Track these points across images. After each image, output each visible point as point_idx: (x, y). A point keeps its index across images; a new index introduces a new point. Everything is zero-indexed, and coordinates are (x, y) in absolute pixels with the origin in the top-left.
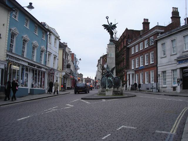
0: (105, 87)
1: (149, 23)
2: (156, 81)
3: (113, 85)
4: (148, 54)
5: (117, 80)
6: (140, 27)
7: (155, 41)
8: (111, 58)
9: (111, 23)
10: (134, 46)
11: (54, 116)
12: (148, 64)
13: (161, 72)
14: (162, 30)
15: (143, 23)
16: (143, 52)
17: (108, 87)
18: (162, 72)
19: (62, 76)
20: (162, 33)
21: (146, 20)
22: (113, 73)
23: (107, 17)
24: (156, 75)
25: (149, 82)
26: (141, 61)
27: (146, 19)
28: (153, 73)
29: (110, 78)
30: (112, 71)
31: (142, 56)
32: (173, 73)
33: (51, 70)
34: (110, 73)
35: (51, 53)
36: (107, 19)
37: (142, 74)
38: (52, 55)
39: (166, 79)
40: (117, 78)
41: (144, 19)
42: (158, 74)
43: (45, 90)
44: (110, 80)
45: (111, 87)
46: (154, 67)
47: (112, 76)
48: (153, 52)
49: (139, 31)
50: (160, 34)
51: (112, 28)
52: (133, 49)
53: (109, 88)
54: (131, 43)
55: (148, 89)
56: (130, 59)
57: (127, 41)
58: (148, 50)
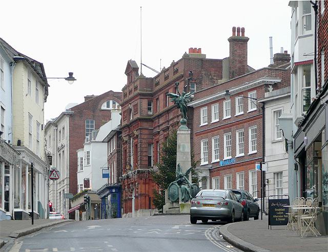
0: (177, 201)
1: (247, 40)
4: (243, 130)
6: (218, 50)
8: (184, 153)
10: (208, 104)
12: (243, 154)
13: (273, 173)
14: (276, 77)
15: (231, 40)
16: (232, 125)
17: (183, 200)
18: (274, 173)
20: (275, 86)
21: (238, 32)
26: (225, 146)
27: (239, 29)
29: (186, 187)
30: (187, 175)
31: (230, 134)
32: (278, 179)
33: (52, 172)
37: (229, 179)
39: (282, 189)
41: (234, 29)
42: (266, 178)
44: (186, 189)
45: (187, 201)
46: (255, 118)
47: (188, 183)
49: (221, 61)
50: (271, 88)
52: (203, 112)
53: (183, 203)
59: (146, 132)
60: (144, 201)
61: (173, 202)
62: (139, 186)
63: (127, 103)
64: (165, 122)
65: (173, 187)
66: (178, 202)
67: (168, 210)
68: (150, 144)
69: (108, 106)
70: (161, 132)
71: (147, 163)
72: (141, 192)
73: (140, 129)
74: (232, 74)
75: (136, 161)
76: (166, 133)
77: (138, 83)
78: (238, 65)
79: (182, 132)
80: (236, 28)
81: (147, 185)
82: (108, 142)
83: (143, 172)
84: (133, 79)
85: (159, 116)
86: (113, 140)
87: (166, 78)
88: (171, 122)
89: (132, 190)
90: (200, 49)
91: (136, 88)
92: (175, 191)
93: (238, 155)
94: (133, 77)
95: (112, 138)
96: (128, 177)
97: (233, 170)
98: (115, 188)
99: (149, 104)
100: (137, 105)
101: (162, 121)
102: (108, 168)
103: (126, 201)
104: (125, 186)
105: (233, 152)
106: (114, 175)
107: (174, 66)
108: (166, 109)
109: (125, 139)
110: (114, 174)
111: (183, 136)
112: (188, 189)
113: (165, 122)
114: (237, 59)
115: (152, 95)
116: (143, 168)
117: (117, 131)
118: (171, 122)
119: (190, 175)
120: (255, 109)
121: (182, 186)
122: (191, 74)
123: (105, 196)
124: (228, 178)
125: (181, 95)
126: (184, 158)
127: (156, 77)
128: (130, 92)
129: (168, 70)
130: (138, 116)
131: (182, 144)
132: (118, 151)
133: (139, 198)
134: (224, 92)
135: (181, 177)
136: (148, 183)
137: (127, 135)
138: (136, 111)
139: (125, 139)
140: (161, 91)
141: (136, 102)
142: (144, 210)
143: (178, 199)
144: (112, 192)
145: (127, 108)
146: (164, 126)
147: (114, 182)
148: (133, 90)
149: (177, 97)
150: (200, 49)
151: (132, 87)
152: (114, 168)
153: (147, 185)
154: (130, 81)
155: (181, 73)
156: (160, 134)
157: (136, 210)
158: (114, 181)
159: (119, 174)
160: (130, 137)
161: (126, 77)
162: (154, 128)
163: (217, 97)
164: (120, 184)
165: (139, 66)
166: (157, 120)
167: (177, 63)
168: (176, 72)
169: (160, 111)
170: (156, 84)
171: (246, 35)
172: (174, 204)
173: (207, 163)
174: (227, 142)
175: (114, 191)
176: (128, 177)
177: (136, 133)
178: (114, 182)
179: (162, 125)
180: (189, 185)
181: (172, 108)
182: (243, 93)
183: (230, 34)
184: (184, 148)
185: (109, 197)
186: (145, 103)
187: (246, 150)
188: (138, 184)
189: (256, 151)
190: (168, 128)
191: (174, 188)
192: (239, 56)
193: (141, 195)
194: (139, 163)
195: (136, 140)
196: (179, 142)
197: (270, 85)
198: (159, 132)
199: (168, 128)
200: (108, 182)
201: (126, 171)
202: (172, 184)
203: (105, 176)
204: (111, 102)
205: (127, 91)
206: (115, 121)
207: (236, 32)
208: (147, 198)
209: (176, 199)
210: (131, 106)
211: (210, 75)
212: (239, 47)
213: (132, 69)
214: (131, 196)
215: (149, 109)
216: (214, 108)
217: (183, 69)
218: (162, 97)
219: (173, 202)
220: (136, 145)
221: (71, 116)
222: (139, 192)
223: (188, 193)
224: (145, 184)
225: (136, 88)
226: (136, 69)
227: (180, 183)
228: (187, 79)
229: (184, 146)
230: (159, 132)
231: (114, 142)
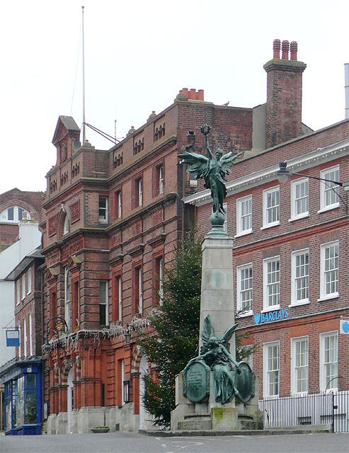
0: (205, 401)
1: (301, 68)
3: (234, 391)
4: (306, 251)
5: (246, 376)
12: (306, 301)
15: (271, 68)
17: (218, 399)
21: (285, 51)
22: (228, 346)
25: (314, 387)
27: (285, 43)
28: (335, 348)
29: (226, 369)
34: (220, 351)
37: (274, 351)
41: (277, 43)
45: (228, 401)
48: (335, 244)
52: (242, 208)
53: (219, 405)
55: (305, 421)
59: (95, 258)
61: (193, 404)
62: (83, 363)
63: (57, 202)
64: (136, 238)
65: (196, 368)
66: (207, 403)
67: (183, 420)
68: (103, 281)
69: (11, 217)
70: (127, 258)
71: (97, 318)
72: (86, 373)
73: (85, 251)
74: (272, 139)
75: (75, 315)
76: (136, 260)
77: (80, 160)
78: (285, 120)
79: (214, 244)
80: (282, 42)
81: (98, 362)
82: (15, 280)
83: (90, 336)
84: (69, 153)
85: (124, 225)
86: (27, 276)
87: (138, 148)
88: (149, 238)
89: (67, 370)
90: (201, 92)
91: (75, 171)
92: (199, 377)
93: (295, 302)
94: (69, 149)
95: (25, 271)
96: (59, 345)
97: (282, 333)
98: (33, 364)
99: (102, 204)
100: (77, 204)
101: (127, 235)
102: (17, 328)
103: (55, 390)
104: (53, 362)
105: (283, 294)
106: (28, 341)
107: (155, 122)
108: (137, 210)
109: (54, 272)
110: (29, 339)
111: (217, 253)
112: (230, 374)
113: (136, 238)
114: (283, 107)
115: (107, 185)
116: (91, 327)
117: (35, 258)
118: (149, 238)
119: (232, 342)
120: (337, 205)
121: (218, 367)
123: (12, 380)
124: (270, 348)
125: (214, 156)
126: (220, 303)
127: (114, 150)
128: (63, 180)
129: (141, 131)
130: (80, 226)
131: (214, 271)
132: (39, 297)
133: (83, 386)
134: (275, 168)
135: (213, 345)
136: (101, 358)
137: (57, 265)
138: (76, 217)
139: (54, 272)
140: (125, 176)
141: (76, 199)
142: (93, 409)
143: (208, 395)
144: (26, 374)
145: (58, 211)
146: (132, 246)
147: (29, 354)
148: (69, 176)
149: (203, 161)
150: (201, 92)
151: (67, 169)
152: (28, 328)
153: (98, 362)
154: (63, 158)
155: (171, 133)
156: (125, 261)
157: (76, 406)
158: (29, 352)
159: (39, 341)
160: (63, 269)
161: (54, 150)
162: (112, 250)
163: (249, 183)
164: (40, 357)
165: (80, 126)
166: (118, 235)
167: (162, 115)
168: (160, 133)
169: (145, 205)
170: (115, 163)
171: (301, 57)
172: (198, 407)
174: (242, 282)
175: (29, 370)
176: (59, 345)
177: (76, 259)
178: (29, 354)
179: (149, 232)
180: (231, 366)
181: (150, 209)
182: (311, 172)
183: (269, 56)
184: (218, 281)
185: (21, 380)
186: (93, 199)
187: (314, 292)
188: (81, 358)
189: (336, 295)
190: (142, 249)
191: (198, 371)
192: (287, 101)
193: (86, 380)
194: (82, 319)
195: (77, 274)
196: (206, 266)
198: (122, 258)
199: (142, 249)
200: (17, 354)
201: (54, 332)
202: (194, 363)
203: (11, 342)
204: (16, 210)
205: (57, 178)
206: (31, 239)
207: (281, 51)
208: (98, 385)
209: (203, 395)
210: (65, 207)
211: (229, 140)
212: (287, 82)
213: (66, 134)
214: (66, 381)
215: (102, 213)
216: (297, 189)
217: (176, 124)
218: (127, 187)
219: (193, 404)
220: (77, 284)
222: (83, 374)
223: (230, 382)
224: (94, 358)
225: (75, 171)
226: (75, 133)
227: (211, 360)
229: (219, 274)
230: (122, 258)
231: (29, 281)
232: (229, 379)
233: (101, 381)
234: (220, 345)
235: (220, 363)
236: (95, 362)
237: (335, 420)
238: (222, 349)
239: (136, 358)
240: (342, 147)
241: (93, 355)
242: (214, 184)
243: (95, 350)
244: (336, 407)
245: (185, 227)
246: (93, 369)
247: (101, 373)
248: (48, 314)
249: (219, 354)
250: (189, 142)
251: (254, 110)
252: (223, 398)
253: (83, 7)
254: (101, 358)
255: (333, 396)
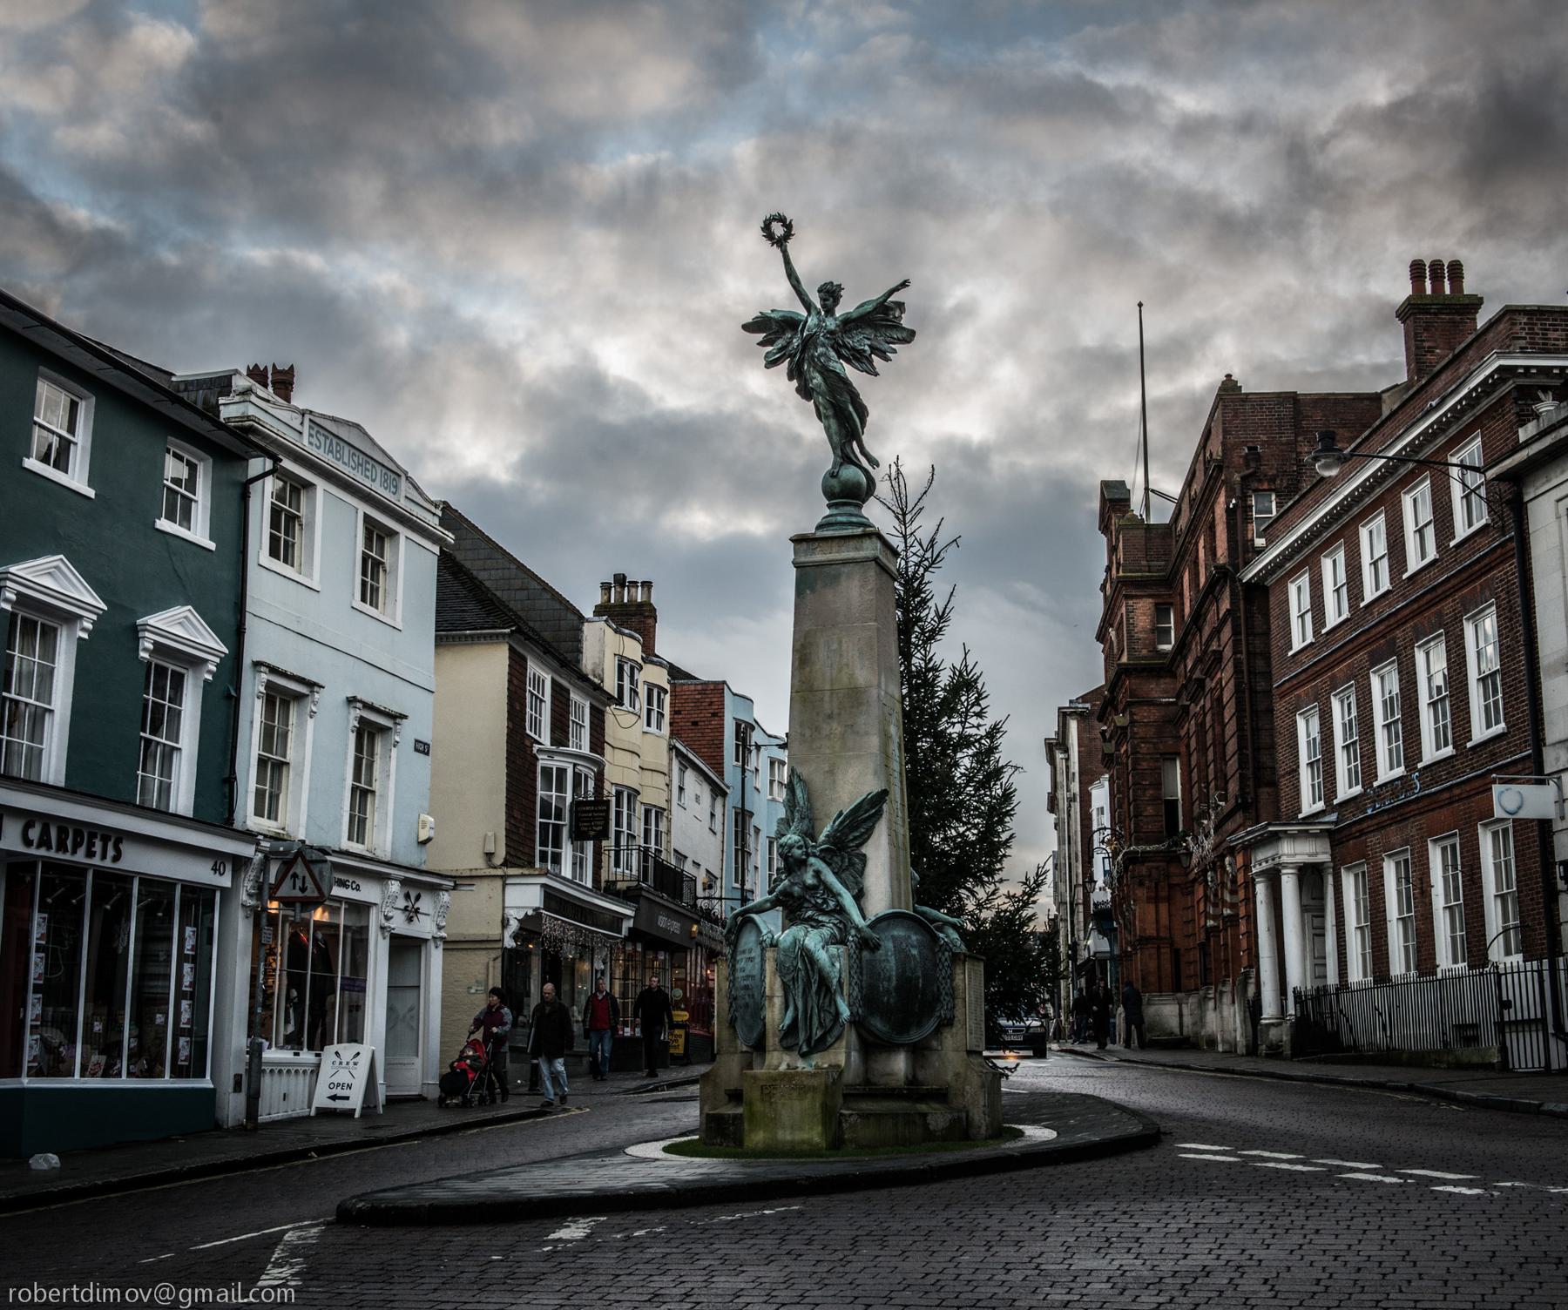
2: (1542, 932)
7: (1504, 487)
9: (831, 294)
11: (1302, 1227)
19: (505, 923)
21: (1437, 278)
23: (778, 229)
24: (1536, 865)
27: (1436, 266)
29: (813, 940)
34: (809, 879)
35: (311, 685)
36: (781, 243)
38: (329, 701)
40: (899, 932)
43: (210, 1094)
44: (807, 956)
51: (837, 348)
52: (1297, 595)
54: (1272, 531)
56: (1280, 706)
57: (1238, 518)
58: (1435, 596)
60: (1152, 965)
97: (1411, 829)
122: (1253, 455)
136: (1169, 899)
153: (1163, 908)
171: (1468, 288)
173: (1320, 805)
197: (1545, 389)
208: (1165, 951)
213: (1229, 376)
221: (1082, 716)
223: (824, 981)
224: (1155, 900)
228: (1237, 477)
232: (820, 971)
233: (1172, 944)
234: (812, 860)
235: (810, 919)
236: (1157, 907)
237: (1508, 1035)
238: (817, 874)
239: (1228, 897)
240: (1472, 385)
241: (1153, 894)
242: (817, 380)
243: (1157, 884)
244: (1506, 1005)
245: (1247, 628)
246: (1154, 920)
247: (1170, 929)
248: (587, 808)
249: (807, 888)
250: (1248, 467)
251: (1385, 396)
252: (802, 1037)
253: (1140, 305)
254: (1169, 899)
255: (1499, 975)
